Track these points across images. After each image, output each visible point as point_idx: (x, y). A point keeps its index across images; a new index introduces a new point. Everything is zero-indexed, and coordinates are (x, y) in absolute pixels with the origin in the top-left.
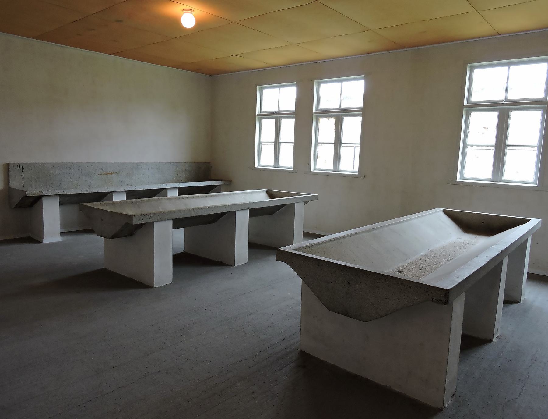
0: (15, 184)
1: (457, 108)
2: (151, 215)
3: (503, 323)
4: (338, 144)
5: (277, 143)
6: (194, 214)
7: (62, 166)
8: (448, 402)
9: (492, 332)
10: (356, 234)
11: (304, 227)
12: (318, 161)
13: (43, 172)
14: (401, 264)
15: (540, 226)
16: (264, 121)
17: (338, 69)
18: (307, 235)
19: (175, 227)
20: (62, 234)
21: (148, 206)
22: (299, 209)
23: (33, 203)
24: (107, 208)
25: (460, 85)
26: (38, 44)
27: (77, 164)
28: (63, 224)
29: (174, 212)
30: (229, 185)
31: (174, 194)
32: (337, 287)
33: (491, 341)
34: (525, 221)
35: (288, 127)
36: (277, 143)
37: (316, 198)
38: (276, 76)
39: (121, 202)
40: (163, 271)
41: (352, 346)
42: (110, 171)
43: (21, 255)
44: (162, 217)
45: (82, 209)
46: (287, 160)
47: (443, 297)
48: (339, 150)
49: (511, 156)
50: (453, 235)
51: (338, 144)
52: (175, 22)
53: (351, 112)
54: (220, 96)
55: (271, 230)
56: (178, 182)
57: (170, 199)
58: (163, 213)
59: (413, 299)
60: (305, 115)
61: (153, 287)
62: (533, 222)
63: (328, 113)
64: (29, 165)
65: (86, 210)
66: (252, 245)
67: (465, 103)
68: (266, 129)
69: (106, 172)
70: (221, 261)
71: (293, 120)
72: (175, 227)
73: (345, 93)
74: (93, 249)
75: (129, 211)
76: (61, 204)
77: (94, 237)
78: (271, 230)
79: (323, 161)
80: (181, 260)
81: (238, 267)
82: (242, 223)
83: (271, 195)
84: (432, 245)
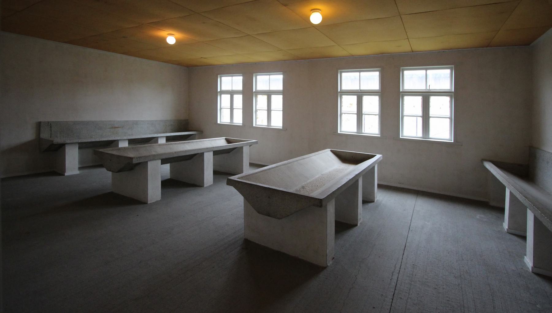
0: (45, 135)
1: (334, 94)
2: (145, 157)
3: (363, 214)
4: (269, 110)
5: (232, 109)
6: (175, 155)
7: (83, 123)
8: (330, 263)
9: (357, 220)
10: (277, 167)
11: (250, 159)
12: (257, 120)
13: (68, 128)
14: (304, 184)
15: (382, 158)
16: (223, 96)
17: (268, 68)
18: (252, 165)
19: (162, 164)
20: (80, 168)
21: (144, 151)
22: (246, 150)
23: (60, 148)
24: (115, 153)
25: (335, 82)
26: (66, 46)
27: (93, 122)
28: (80, 162)
29: (162, 154)
30: (202, 134)
31: (162, 141)
32: (264, 200)
33: (357, 225)
34: (373, 156)
35: (238, 100)
36: (232, 109)
37: (256, 143)
38: (230, 70)
39: (124, 148)
40: (154, 191)
41: (276, 234)
42: (116, 126)
43: (48, 185)
44: (154, 158)
45: (96, 153)
46: (238, 120)
47: (318, 204)
48: (271, 113)
49: (366, 119)
50: (336, 165)
51: (269, 110)
52: (164, 40)
53: (276, 92)
54: (195, 81)
55: (227, 164)
56: (166, 132)
57: (160, 145)
58: (154, 155)
59: (305, 205)
60: (248, 93)
61: (147, 203)
62: (378, 156)
63: (263, 93)
64: (56, 123)
65: (99, 153)
66: (216, 173)
67: (339, 90)
68: (224, 101)
69: (114, 127)
70: (195, 184)
71: (241, 96)
72: (162, 164)
73: (273, 81)
74: (103, 178)
75: (131, 155)
76: (79, 148)
77: (104, 170)
78: (227, 164)
79: (260, 120)
80: (166, 184)
81: (207, 187)
82: (209, 161)
83: (228, 141)
84: (324, 170)
